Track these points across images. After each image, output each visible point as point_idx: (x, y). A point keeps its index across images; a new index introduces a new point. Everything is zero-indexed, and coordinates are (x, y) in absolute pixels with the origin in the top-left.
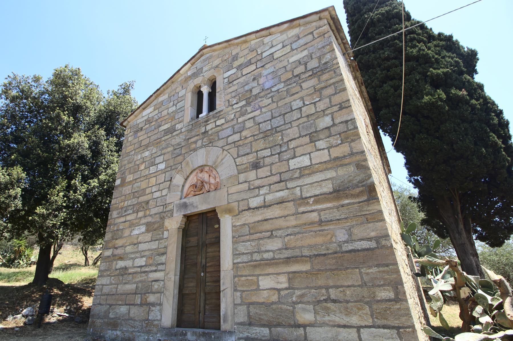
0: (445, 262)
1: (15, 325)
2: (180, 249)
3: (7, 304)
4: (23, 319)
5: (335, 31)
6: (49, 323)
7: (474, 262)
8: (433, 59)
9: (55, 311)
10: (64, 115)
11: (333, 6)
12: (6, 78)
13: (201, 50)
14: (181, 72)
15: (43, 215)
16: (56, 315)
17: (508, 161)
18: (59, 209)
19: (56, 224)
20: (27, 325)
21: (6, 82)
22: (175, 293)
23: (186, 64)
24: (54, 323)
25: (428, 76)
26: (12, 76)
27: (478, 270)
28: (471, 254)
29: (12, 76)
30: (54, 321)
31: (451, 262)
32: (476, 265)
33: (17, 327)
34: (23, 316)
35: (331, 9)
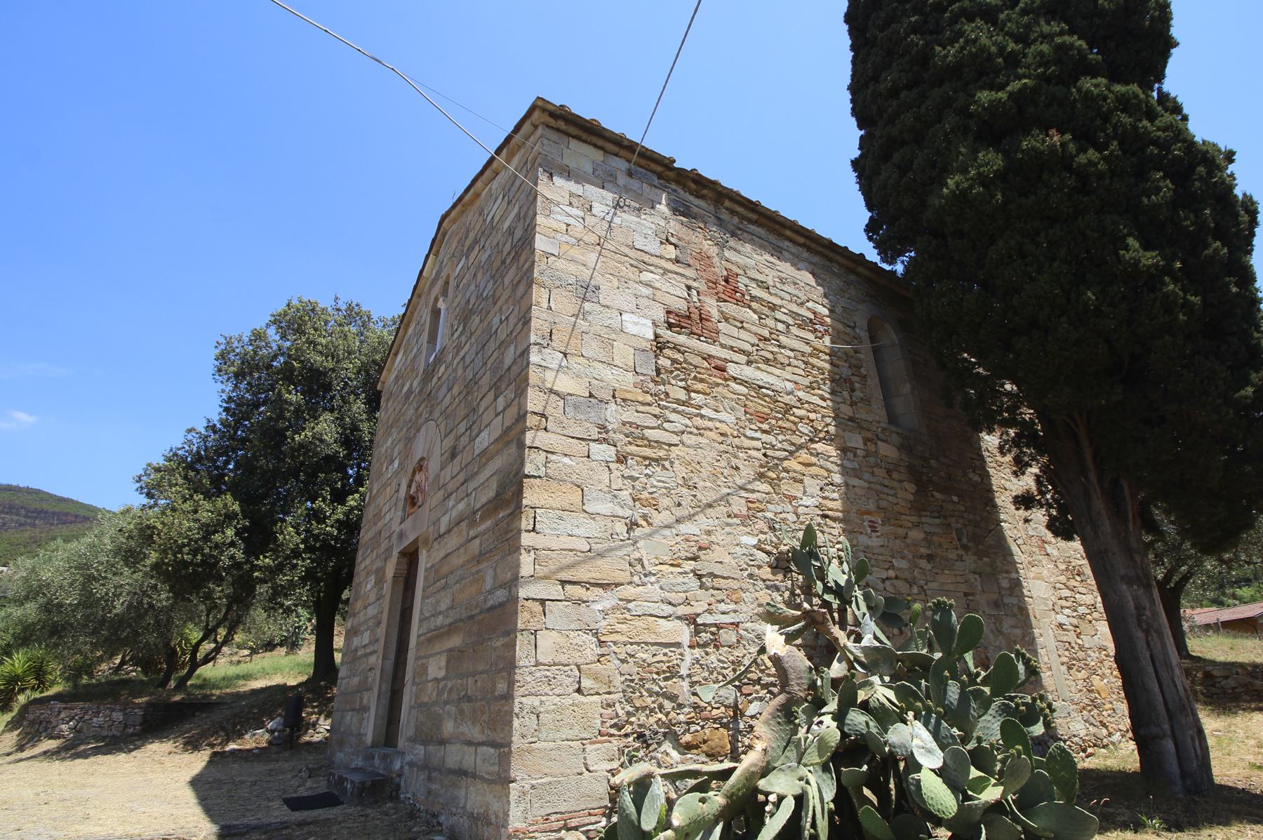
0: (799, 613)
1: (254, 745)
2: (398, 613)
3: (254, 714)
4: (267, 736)
5: (585, 136)
6: (309, 743)
7: (1130, 598)
8: (1000, 60)
9: (320, 722)
10: (290, 393)
11: (538, 98)
12: (216, 347)
13: (440, 224)
14: (424, 274)
15: (268, 568)
16: (322, 730)
17: (1186, 305)
18: (296, 553)
19: (292, 580)
20: (273, 745)
21: (217, 351)
22: (384, 688)
23: (427, 257)
24: (320, 742)
25: (971, 116)
26: (222, 340)
27: (1139, 622)
28: (1123, 578)
29: (222, 340)
30: (318, 739)
31: (814, 614)
32: (1137, 608)
33: (257, 748)
34: (267, 731)
35: (540, 103)
